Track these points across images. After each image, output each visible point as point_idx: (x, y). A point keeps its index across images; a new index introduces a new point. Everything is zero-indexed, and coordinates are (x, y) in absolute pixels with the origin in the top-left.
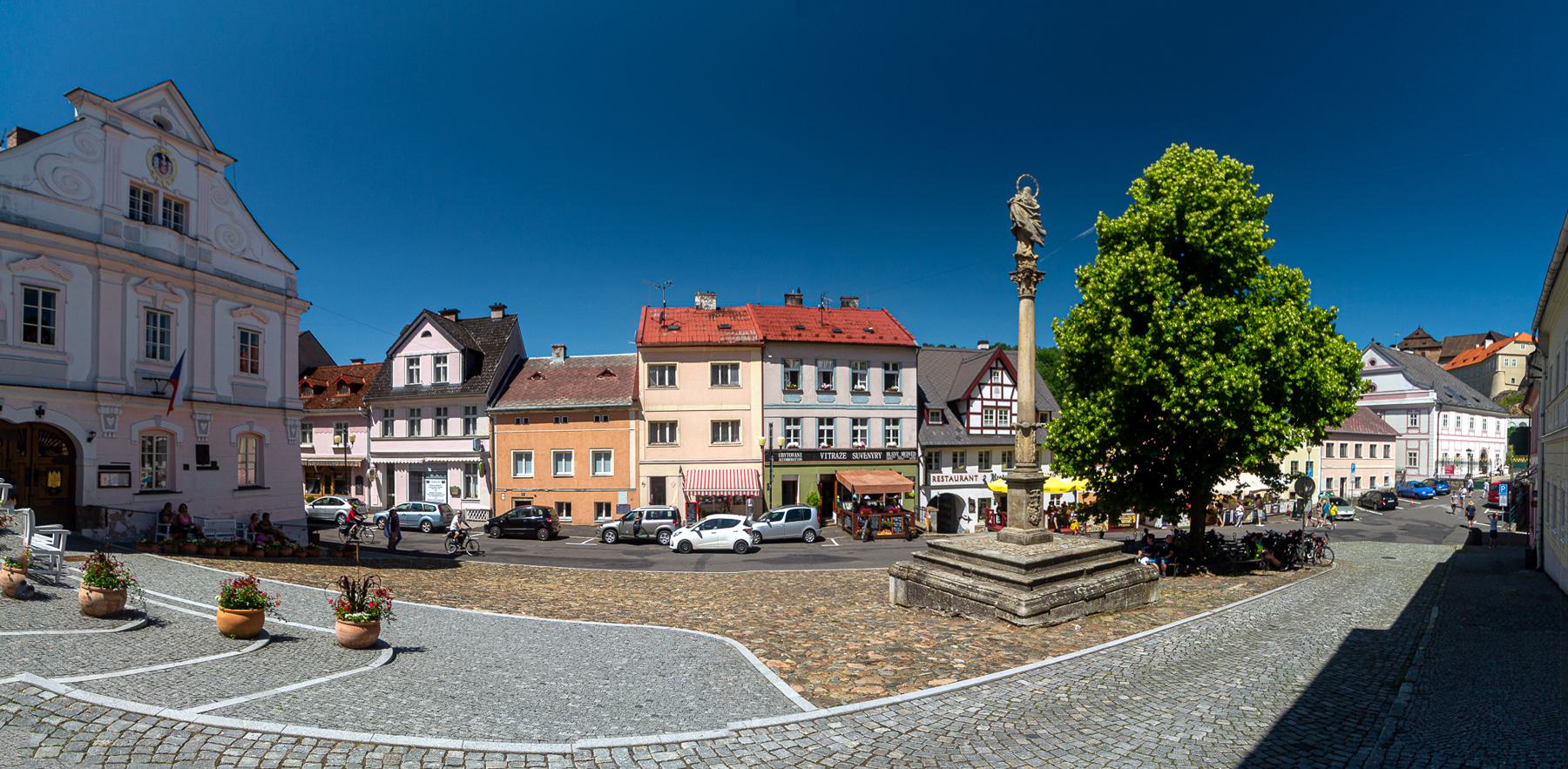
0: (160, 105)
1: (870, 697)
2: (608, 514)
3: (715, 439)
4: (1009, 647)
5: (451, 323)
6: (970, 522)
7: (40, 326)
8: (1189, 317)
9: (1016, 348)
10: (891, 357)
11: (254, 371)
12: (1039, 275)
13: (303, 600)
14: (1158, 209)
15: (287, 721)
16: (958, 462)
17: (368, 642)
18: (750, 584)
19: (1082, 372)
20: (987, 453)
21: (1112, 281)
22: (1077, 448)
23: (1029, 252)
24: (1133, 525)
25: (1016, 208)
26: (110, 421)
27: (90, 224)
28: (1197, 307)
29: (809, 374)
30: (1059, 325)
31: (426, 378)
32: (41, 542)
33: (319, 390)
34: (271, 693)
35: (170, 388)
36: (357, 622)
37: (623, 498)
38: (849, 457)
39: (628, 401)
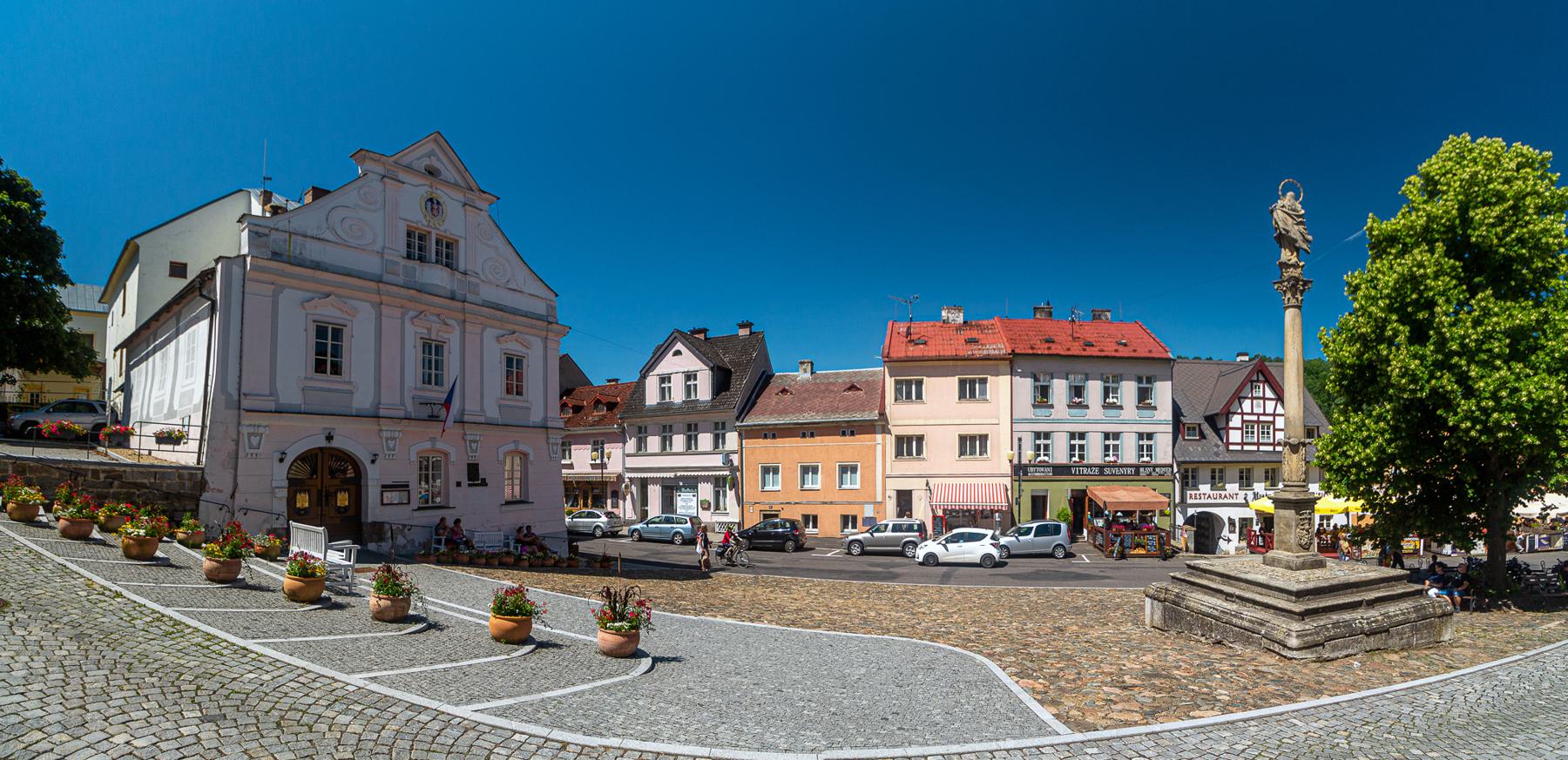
0: (429, 155)
1: (1127, 724)
2: (854, 527)
3: (962, 453)
4: (1278, 681)
5: (700, 342)
6: (1230, 543)
7: (329, 359)
8: (1477, 323)
9: (1280, 360)
10: (1145, 370)
11: (519, 393)
12: (1305, 283)
13: (568, 609)
14: (1436, 208)
15: (553, 726)
16: (1217, 479)
17: (628, 651)
18: (998, 600)
19: (1359, 383)
20: (1249, 470)
21: (1387, 286)
22: (1349, 467)
23: (1294, 259)
24: (1416, 552)
25: (1279, 215)
26: (391, 444)
27: (372, 265)
28: (1486, 313)
29: (1059, 388)
30: (1326, 333)
31: (678, 396)
32: (335, 557)
33: (577, 409)
34: (537, 697)
35: (443, 412)
36: (618, 631)
37: (869, 511)
38: (1102, 473)
39: (875, 415)
